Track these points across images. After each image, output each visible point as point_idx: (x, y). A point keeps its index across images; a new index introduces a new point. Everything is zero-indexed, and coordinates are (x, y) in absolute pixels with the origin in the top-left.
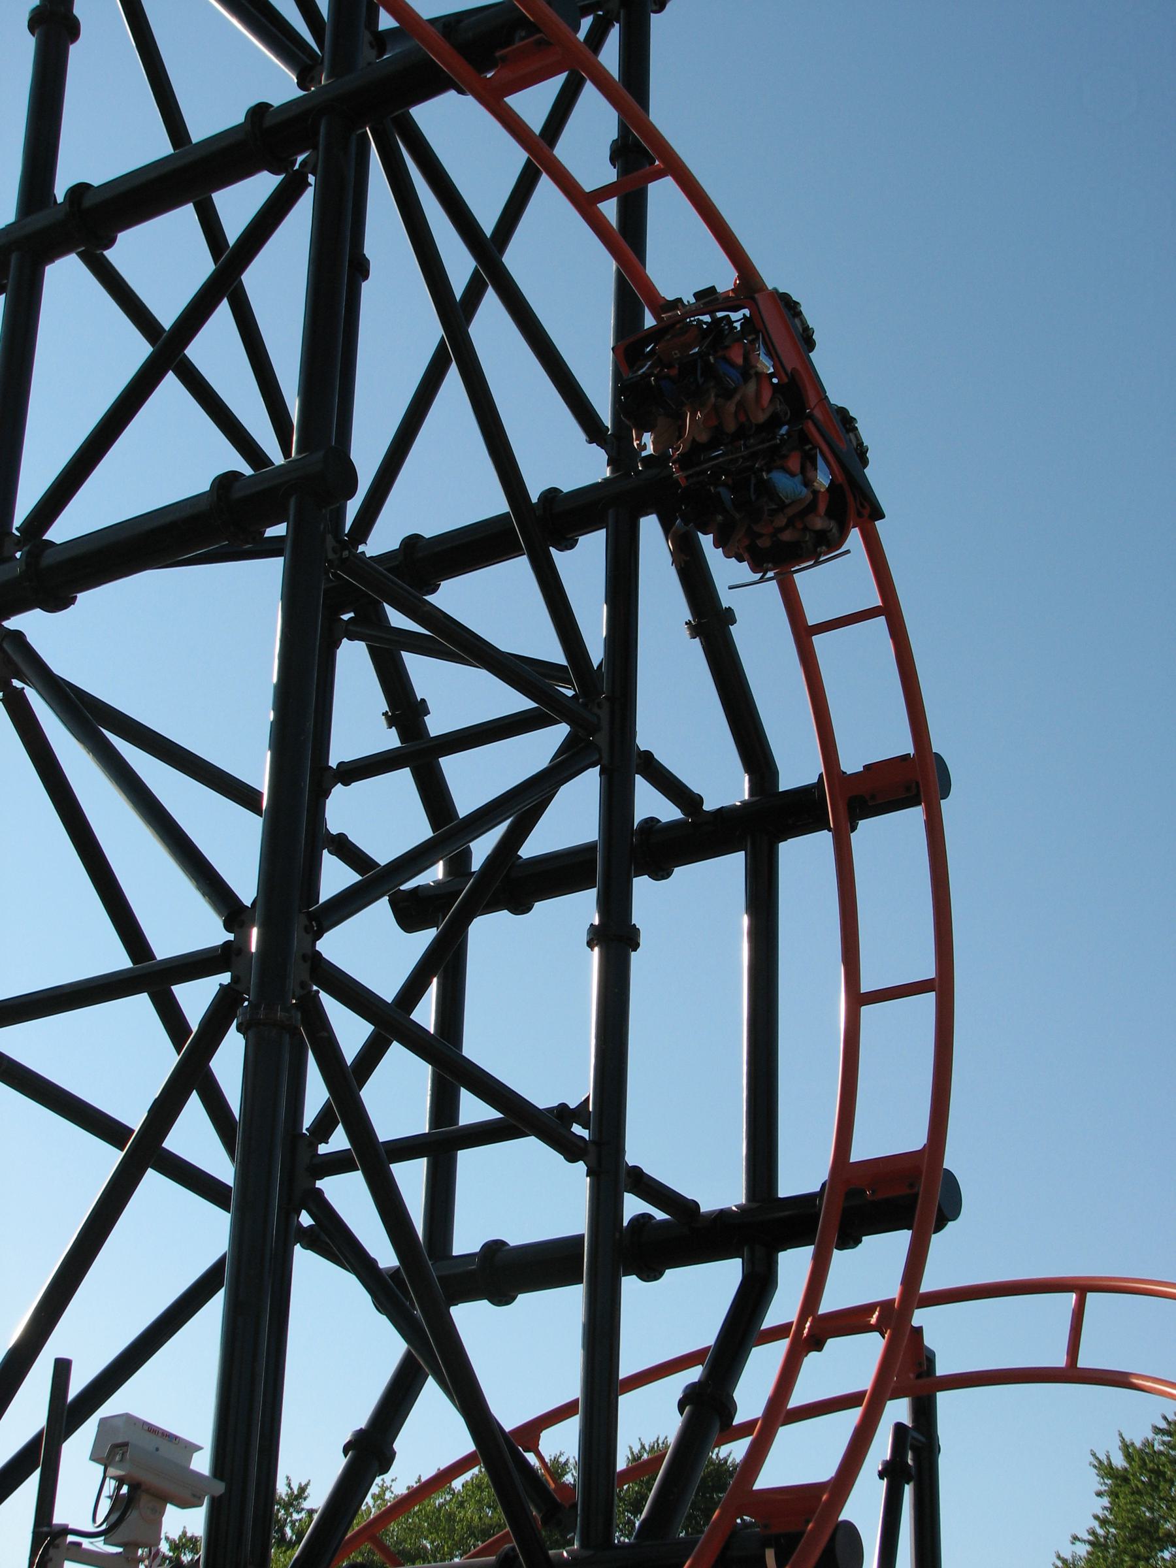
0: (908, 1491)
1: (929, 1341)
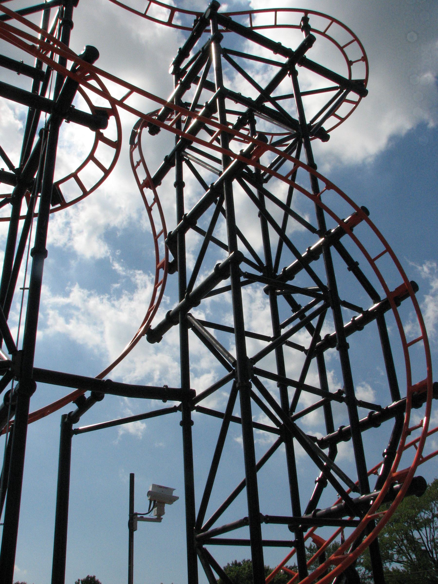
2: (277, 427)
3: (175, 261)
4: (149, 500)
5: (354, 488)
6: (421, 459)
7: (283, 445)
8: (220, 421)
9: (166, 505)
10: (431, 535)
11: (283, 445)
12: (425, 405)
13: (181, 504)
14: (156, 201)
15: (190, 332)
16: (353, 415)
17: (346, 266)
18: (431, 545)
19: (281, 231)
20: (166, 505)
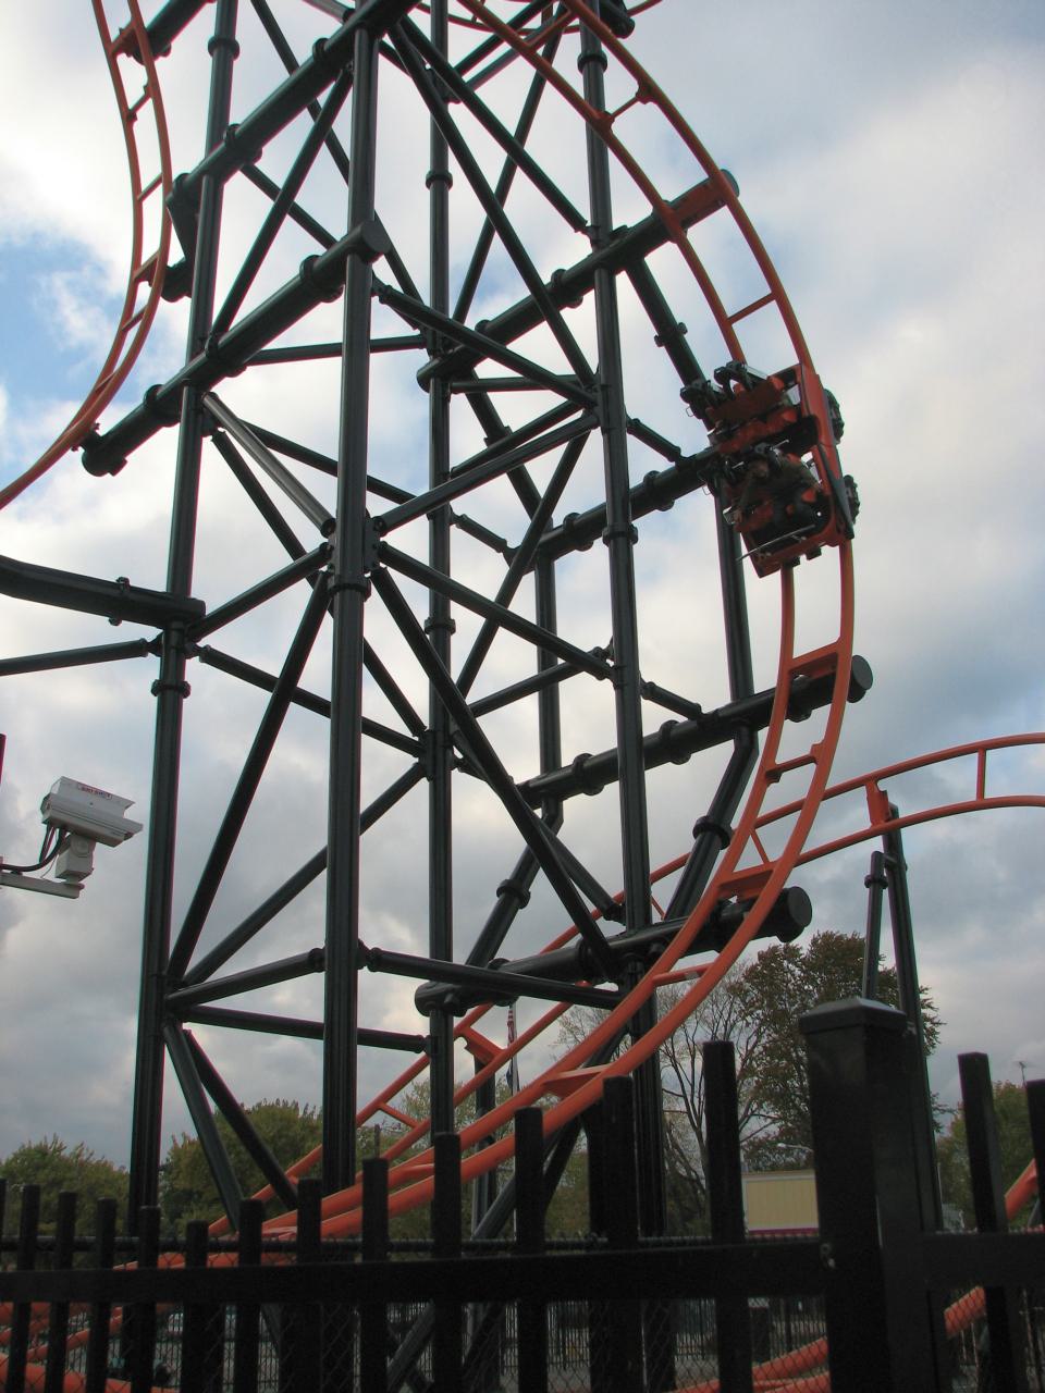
0: (886, 893)
1: (893, 799)
2: (414, 735)
3: (184, 267)
4: (44, 822)
5: (612, 910)
7: (423, 787)
8: (264, 697)
9: (98, 844)
11: (423, 787)
13: (139, 847)
14: (152, 94)
15: (208, 448)
16: (628, 717)
17: (652, 331)
19: (493, 201)
20: (98, 844)
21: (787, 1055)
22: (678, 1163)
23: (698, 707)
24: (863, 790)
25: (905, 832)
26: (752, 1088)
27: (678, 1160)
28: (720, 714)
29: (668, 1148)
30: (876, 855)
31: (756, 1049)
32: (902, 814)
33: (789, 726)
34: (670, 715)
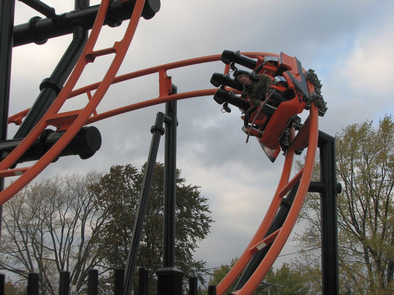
0: (163, 138)
1: (174, 82)
6: (92, 115)
10: (68, 241)
12: (126, 23)
18: (64, 255)
21: (119, 231)
22: (47, 291)
23: (53, 10)
24: (156, 75)
25: (179, 102)
26: (96, 249)
27: (46, 288)
28: (67, 17)
29: (41, 281)
30: (160, 115)
31: (102, 226)
32: (179, 92)
33: (105, 29)
34: (35, 13)
